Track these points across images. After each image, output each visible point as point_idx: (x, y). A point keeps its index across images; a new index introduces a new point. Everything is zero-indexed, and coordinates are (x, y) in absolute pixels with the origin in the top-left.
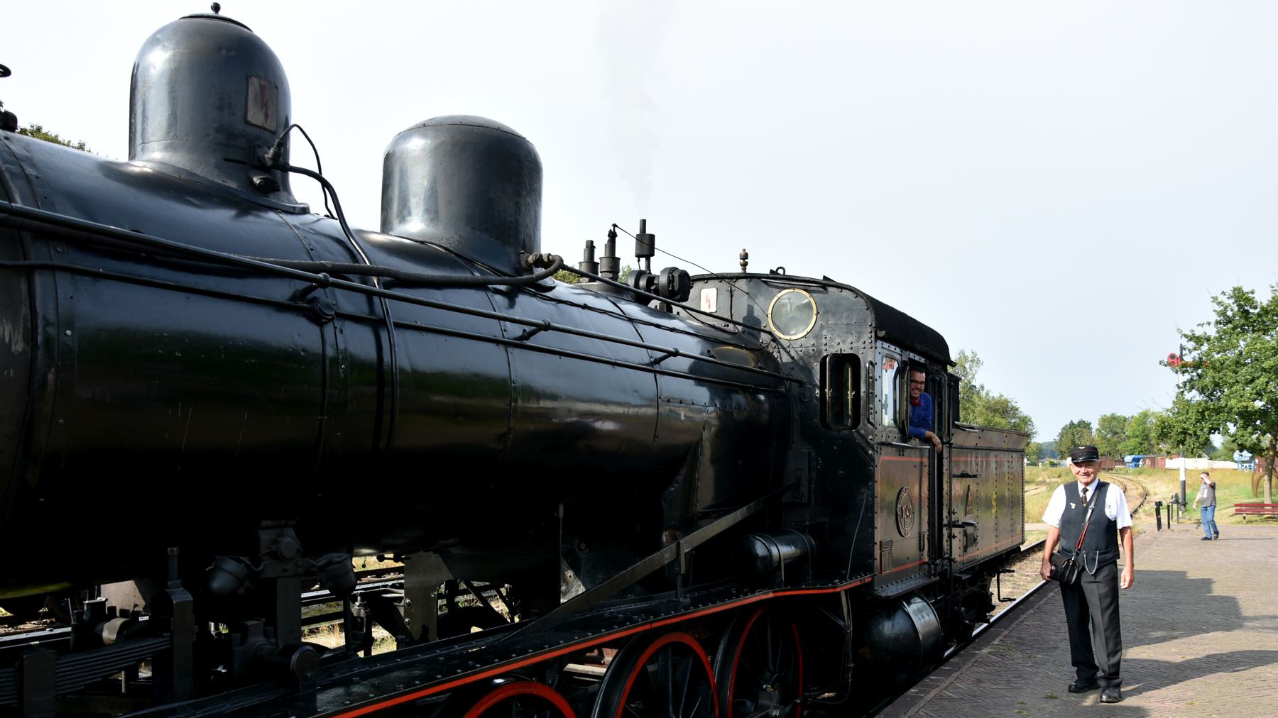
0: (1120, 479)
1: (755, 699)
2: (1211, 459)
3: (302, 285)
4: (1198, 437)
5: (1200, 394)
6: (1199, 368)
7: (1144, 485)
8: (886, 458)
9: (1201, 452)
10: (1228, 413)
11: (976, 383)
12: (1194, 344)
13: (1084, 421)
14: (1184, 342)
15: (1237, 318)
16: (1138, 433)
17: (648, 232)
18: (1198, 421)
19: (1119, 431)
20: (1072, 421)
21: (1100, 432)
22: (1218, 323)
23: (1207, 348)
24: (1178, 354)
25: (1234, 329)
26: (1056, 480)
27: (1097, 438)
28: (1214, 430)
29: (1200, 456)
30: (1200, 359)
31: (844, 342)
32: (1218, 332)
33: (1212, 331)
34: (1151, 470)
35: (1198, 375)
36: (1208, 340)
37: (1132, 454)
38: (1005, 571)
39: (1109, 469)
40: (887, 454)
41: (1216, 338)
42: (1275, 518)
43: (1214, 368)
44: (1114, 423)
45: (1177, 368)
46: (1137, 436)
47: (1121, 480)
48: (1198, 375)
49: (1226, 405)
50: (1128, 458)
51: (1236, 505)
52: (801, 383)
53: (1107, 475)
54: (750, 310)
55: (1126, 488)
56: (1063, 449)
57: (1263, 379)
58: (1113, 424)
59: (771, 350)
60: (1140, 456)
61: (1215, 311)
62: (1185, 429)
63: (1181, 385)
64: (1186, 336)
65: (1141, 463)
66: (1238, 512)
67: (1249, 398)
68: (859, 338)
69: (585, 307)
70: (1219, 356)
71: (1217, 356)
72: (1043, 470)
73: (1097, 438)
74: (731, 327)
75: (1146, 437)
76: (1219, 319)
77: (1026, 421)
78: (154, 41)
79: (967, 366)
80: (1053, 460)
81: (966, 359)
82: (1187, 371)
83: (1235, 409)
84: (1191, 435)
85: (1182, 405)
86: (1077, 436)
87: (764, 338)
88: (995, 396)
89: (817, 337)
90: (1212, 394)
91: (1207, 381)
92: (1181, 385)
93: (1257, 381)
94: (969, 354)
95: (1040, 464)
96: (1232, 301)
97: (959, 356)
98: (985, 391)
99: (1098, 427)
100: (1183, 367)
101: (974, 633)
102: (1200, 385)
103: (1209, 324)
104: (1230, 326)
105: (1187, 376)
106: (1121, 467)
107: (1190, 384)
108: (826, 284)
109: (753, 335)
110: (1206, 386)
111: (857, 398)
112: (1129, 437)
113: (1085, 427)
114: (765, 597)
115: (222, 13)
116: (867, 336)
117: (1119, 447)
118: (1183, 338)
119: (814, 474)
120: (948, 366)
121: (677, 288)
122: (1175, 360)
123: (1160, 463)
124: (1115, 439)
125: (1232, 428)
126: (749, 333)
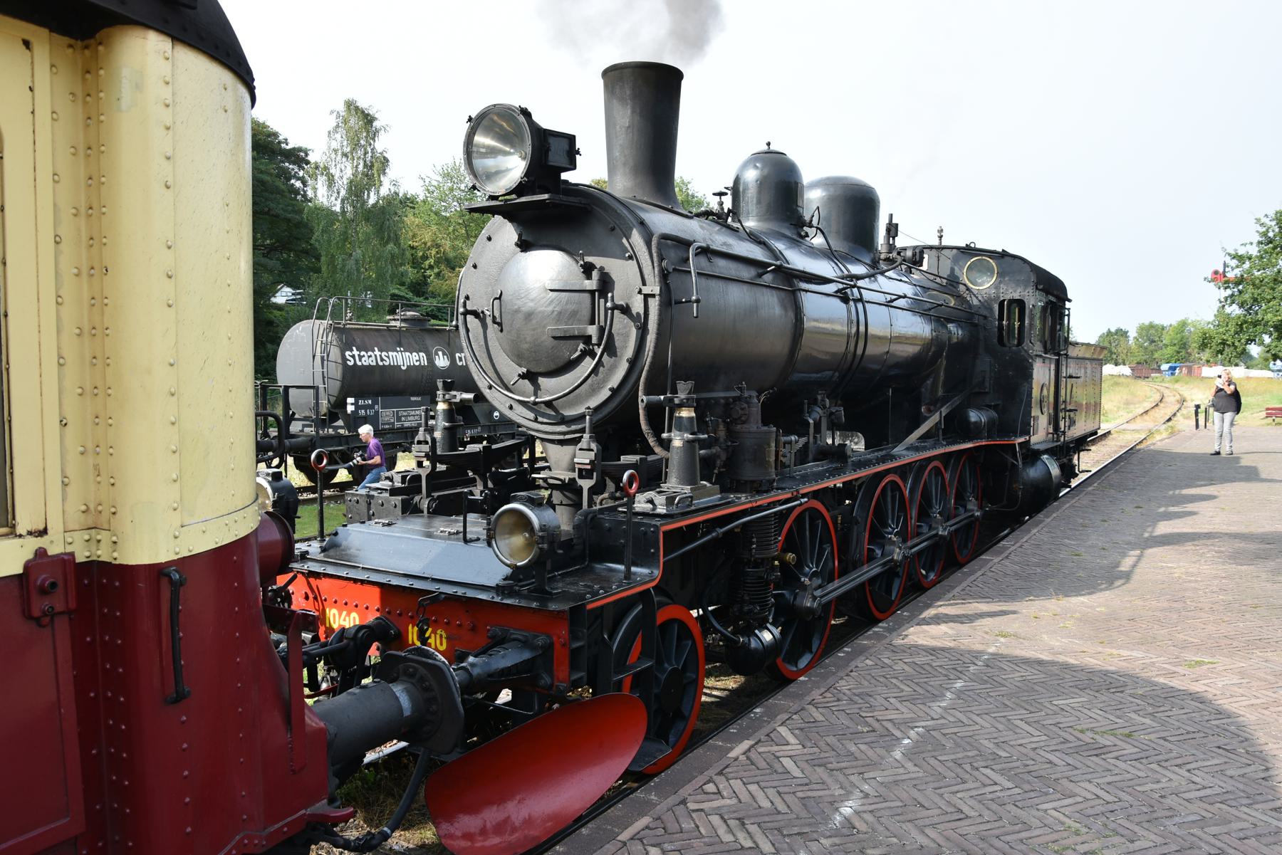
0: (1156, 387)
1: (882, 547)
2: (1248, 368)
3: (841, 286)
4: (1236, 347)
5: (1240, 308)
6: (1240, 284)
7: (1181, 393)
9: (1237, 361)
10: (1264, 326)
12: (1237, 262)
14: (1228, 259)
15: (1278, 238)
16: (1176, 342)
17: (894, 222)
18: (1236, 333)
19: (1157, 339)
22: (1260, 243)
24: (1221, 270)
25: (1275, 248)
27: (1133, 346)
28: (1250, 341)
29: (1237, 365)
30: (1242, 276)
31: (1015, 291)
32: (1259, 251)
33: (1254, 251)
34: (1187, 379)
35: (1239, 290)
38: (1083, 450)
41: (1257, 257)
43: (1254, 285)
44: (1152, 331)
45: (1220, 284)
46: (1175, 345)
47: (1159, 388)
48: (1239, 290)
49: (1263, 319)
50: (1165, 367)
51: (1268, 409)
52: (985, 317)
53: (1144, 383)
58: (1151, 334)
59: (965, 295)
60: (1176, 365)
61: (1258, 232)
63: (1223, 300)
64: (1229, 254)
65: (1177, 371)
70: (1259, 273)
71: (1257, 274)
73: (1133, 346)
74: (938, 280)
75: (1184, 345)
76: (1261, 239)
78: (745, 166)
82: (1228, 287)
83: (1271, 323)
84: (1229, 345)
85: (1223, 319)
86: (1113, 344)
87: (962, 288)
89: (996, 288)
90: (1250, 308)
91: (1247, 296)
92: (1223, 300)
96: (1274, 223)
99: (1136, 335)
100: (1225, 283)
101: (1061, 495)
102: (1241, 300)
103: (1251, 244)
104: (1271, 245)
105: (1229, 292)
106: (1157, 375)
107: (1232, 299)
108: (1004, 254)
109: (952, 286)
110: (1246, 301)
111: (1021, 327)
112: (1166, 346)
113: (1122, 335)
114: (981, 444)
115: (773, 148)
117: (1156, 355)
119: (993, 374)
120: (1067, 302)
121: (918, 259)
122: (1218, 276)
124: (1152, 347)
125: (1267, 339)
126: (950, 285)
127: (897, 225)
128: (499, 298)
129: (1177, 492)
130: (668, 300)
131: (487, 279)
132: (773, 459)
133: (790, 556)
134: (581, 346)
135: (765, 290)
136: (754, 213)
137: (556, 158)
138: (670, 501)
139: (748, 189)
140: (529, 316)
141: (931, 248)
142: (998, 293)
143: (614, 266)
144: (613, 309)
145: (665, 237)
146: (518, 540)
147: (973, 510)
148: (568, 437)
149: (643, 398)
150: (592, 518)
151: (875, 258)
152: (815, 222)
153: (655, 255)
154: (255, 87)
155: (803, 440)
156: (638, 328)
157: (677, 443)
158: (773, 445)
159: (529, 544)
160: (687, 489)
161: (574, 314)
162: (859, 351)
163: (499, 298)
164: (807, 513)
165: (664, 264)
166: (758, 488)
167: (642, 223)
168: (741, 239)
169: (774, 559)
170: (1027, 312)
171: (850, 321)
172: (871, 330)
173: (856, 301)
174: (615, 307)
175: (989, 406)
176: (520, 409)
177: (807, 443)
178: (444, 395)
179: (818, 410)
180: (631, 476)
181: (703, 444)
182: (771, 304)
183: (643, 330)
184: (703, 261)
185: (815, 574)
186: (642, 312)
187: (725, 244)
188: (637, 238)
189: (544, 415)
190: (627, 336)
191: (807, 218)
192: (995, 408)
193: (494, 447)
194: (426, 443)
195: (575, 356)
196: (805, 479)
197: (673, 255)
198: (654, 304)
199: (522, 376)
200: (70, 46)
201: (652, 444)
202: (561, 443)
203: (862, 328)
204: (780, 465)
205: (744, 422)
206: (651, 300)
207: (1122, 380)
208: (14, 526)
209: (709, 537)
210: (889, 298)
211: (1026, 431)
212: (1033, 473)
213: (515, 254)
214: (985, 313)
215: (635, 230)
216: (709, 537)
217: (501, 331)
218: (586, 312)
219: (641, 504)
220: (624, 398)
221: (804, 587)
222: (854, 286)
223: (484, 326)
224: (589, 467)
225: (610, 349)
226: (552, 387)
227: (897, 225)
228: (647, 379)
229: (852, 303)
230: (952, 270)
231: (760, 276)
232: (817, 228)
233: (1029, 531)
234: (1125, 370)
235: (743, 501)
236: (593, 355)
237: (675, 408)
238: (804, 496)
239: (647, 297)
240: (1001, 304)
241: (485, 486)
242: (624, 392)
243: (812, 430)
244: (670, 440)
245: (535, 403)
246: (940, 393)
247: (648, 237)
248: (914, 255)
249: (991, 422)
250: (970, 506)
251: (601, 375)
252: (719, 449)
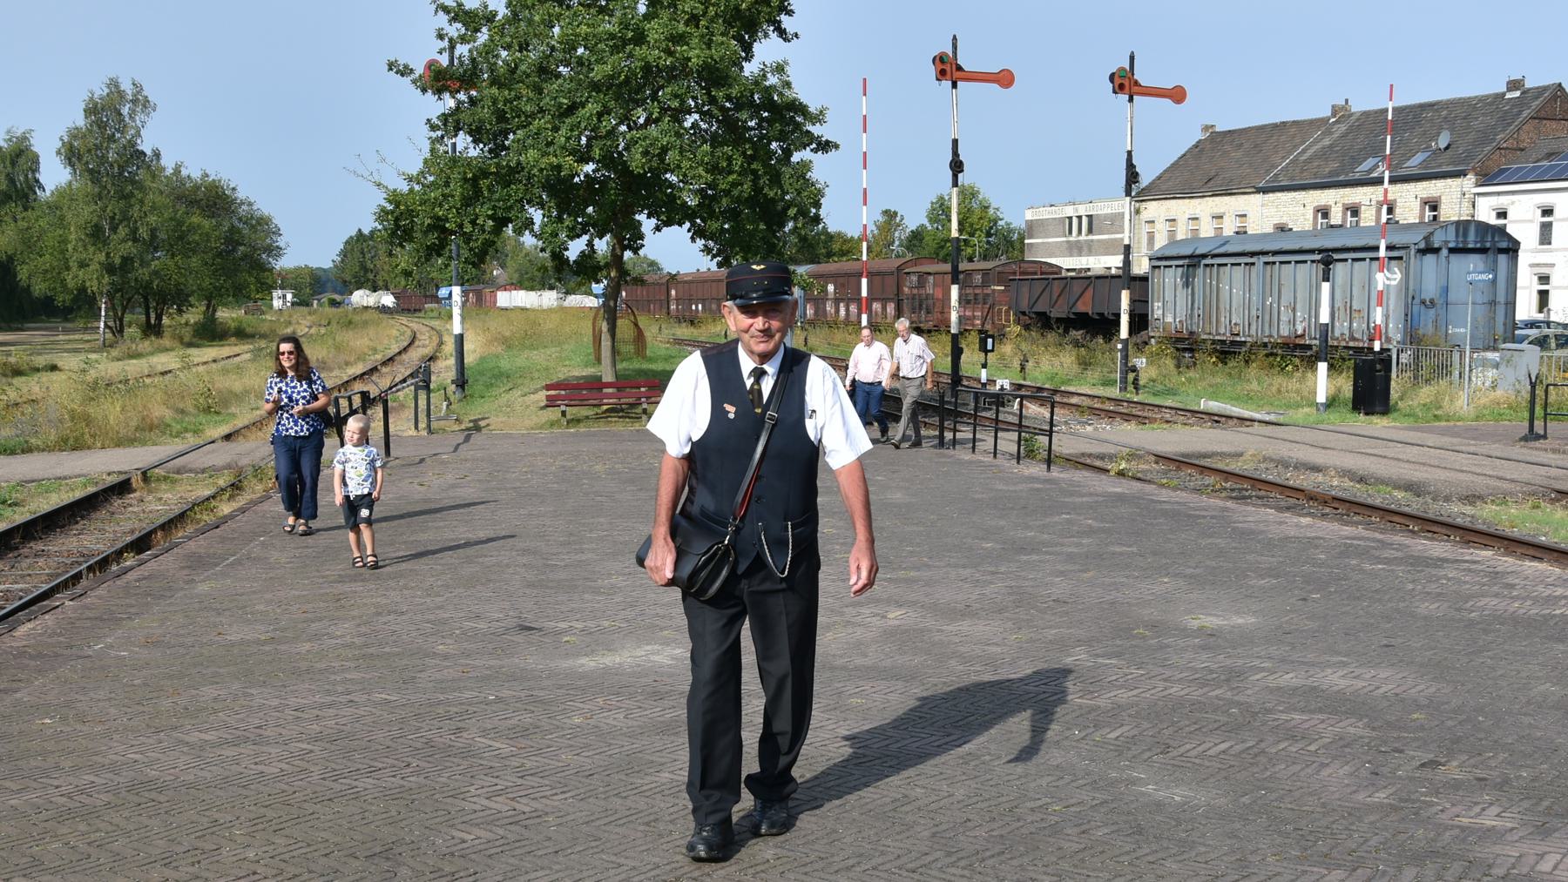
11: (146, 146)
20: (360, 230)
23: (486, 37)
36: (490, 18)
42: (622, 410)
51: (548, 388)
56: (348, 278)
57: (592, 108)
62: (438, 218)
64: (446, 10)
66: (551, 402)
67: (563, 148)
77: (261, 224)
79: (125, 110)
85: (442, 164)
86: (368, 256)
88: (193, 176)
93: (582, 112)
94: (126, 86)
95: (315, 302)
107: (451, 123)
118: (441, 13)
123: (488, 298)
125: (537, 215)
234: (388, 300)
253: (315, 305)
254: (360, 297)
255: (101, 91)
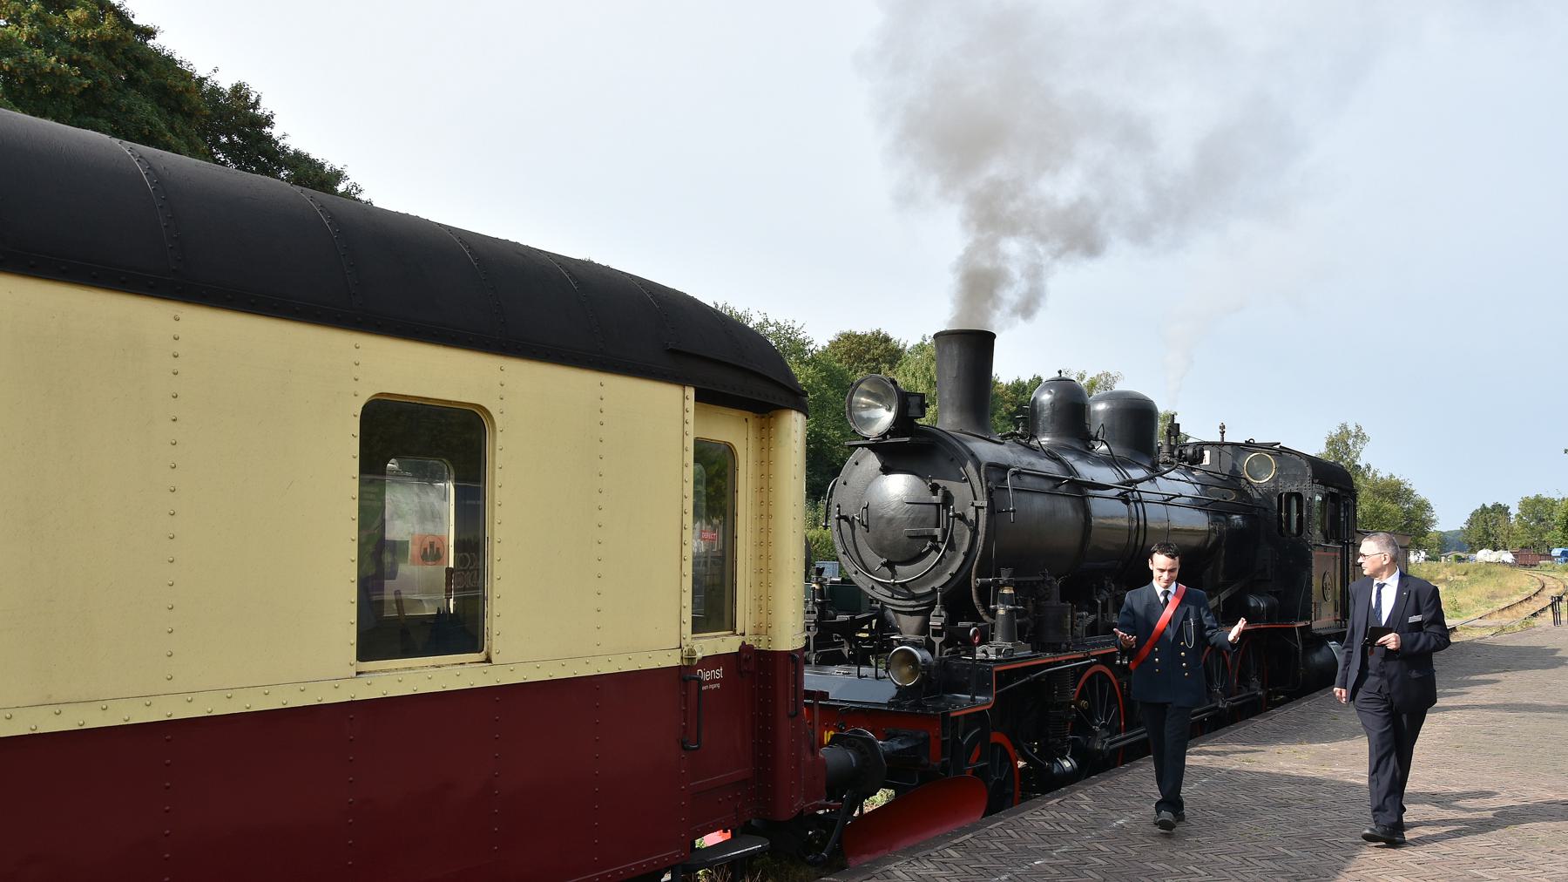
8: (1317, 553)
13: (1500, 505)
20: (1484, 505)
21: (1521, 518)
26: (1461, 578)
27: (1516, 526)
37: (1560, 547)
39: (1531, 565)
40: (1318, 551)
44: (1540, 507)
52: (1265, 509)
53: (1527, 572)
54: (1234, 466)
55: (1544, 587)
58: (1537, 509)
68: (1302, 484)
69: (1179, 480)
72: (1446, 566)
73: (1516, 526)
77: (1423, 506)
79: (1350, 442)
80: (1459, 554)
81: (1349, 434)
88: (1384, 477)
94: (1352, 428)
95: (1443, 558)
97: (1339, 431)
98: (1372, 471)
99: (1518, 512)
115: (1063, 375)
116: (1308, 482)
117: (1546, 538)
124: (1540, 527)
127: (1179, 425)
128: (867, 508)
129: (1465, 678)
130: (992, 510)
131: (856, 493)
132: (1069, 627)
133: (1084, 703)
134: (929, 543)
135: (1060, 497)
136: (1049, 431)
137: (913, 412)
138: (998, 651)
139: (1044, 410)
140: (890, 521)
141: (1213, 444)
142: (1277, 487)
143: (954, 487)
144: (953, 517)
145: (989, 465)
146: (906, 670)
147: (1255, 690)
148: (916, 609)
149: (976, 582)
150: (945, 663)
151: (1154, 462)
152: (1100, 437)
153: (983, 479)
154: (297, 153)
155: (1093, 617)
156: (971, 531)
157: (1001, 612)
158: (1069, 616)
159: (913, 674)
160: (1009, 645)
161: (923, 521)
162: (1140, 542)
163: (867, 508)
164: (1097, 676)
165: (989, 484)
166: (1056, 649)
167: (973, 455)
168: (1041, 458)
169: (1071, 703)
170: (1305, 504)
171: (1130, 519)
172: (1150, 524)
173: (1136, 502)
174: (955, 516)
175: (1270, 593)
176: (879, 589)
177: (1096, 620)
178: (817, 578)
179: (1105, 592)
180: (975, 631)
181: (1020, 614)
182: (1065, 508)
183: (975, 532)
184: (1015, 478)
185: (1102, 726)
186: (974, 519)
187: (1029, 464)
188: (970, 467)
189: (898, 593)
190: (963, 537)
191: (1093, 432)
192: (1276, 594)
193: (857, 617)
194: (814, 612)
195: (925, 550)
196: (1094, 646)
197: (994, 476)
198: (983, 514)
199: (883, 565)
200: (757, 417)
201: (981, 614)
202: (911, 614)
203: (1141, 523)
204: (1075, 637)
205: (1046, 600)
206: (980, 511)
207: (1499, 568)
208: (735, 631)
209: (1024, 680)
210: (1166, 497)
211: (1307, 615)
212: (1318, 658)
213: (878, 476)
214: (1265, 505)
215: (969, 462)
216: (1024, 680)
217: (868, 531)
218: (933, 519)
219: (979, 655)
220: (960, 578)
221: (1095, 733)
222: (1134, 490)
223: (853, 527)
224: (940, 628)
225: (951, 546)
226: (906, 573)
227: (1179, 425)
228: (978, 566)
229: (1132, 504)
230: (1234, 465)
231: (1057, 487)
232: (1102, 441)
233: (1301, 703)
234: (1508, 557)
235: (1048, 657)
236: (938, 550)
237: (999, 587)
238: (1093, 657)
239: (977, 508)
240: (1280, 496)
241: (851, 647)
242: (960, 576)
243: (1100, 608)
244: (995, 610)
245: (894, 584)
246: (1221, 580)
247: (978, 465)
248: (1195, 453)
249: (1271, 608)
250: (1253, 686)
251: (943, 564)
252: (1028, 619)
253: (1443, 561)
254: (1484, 555)
255: (1335, 431)
